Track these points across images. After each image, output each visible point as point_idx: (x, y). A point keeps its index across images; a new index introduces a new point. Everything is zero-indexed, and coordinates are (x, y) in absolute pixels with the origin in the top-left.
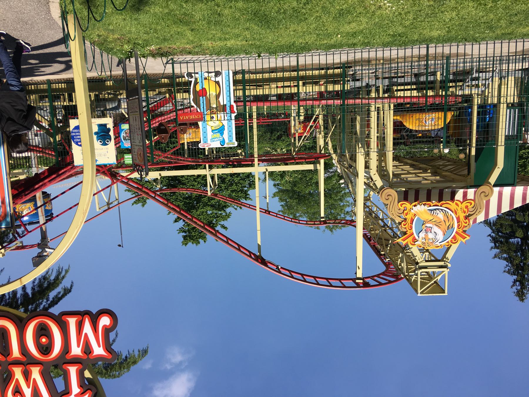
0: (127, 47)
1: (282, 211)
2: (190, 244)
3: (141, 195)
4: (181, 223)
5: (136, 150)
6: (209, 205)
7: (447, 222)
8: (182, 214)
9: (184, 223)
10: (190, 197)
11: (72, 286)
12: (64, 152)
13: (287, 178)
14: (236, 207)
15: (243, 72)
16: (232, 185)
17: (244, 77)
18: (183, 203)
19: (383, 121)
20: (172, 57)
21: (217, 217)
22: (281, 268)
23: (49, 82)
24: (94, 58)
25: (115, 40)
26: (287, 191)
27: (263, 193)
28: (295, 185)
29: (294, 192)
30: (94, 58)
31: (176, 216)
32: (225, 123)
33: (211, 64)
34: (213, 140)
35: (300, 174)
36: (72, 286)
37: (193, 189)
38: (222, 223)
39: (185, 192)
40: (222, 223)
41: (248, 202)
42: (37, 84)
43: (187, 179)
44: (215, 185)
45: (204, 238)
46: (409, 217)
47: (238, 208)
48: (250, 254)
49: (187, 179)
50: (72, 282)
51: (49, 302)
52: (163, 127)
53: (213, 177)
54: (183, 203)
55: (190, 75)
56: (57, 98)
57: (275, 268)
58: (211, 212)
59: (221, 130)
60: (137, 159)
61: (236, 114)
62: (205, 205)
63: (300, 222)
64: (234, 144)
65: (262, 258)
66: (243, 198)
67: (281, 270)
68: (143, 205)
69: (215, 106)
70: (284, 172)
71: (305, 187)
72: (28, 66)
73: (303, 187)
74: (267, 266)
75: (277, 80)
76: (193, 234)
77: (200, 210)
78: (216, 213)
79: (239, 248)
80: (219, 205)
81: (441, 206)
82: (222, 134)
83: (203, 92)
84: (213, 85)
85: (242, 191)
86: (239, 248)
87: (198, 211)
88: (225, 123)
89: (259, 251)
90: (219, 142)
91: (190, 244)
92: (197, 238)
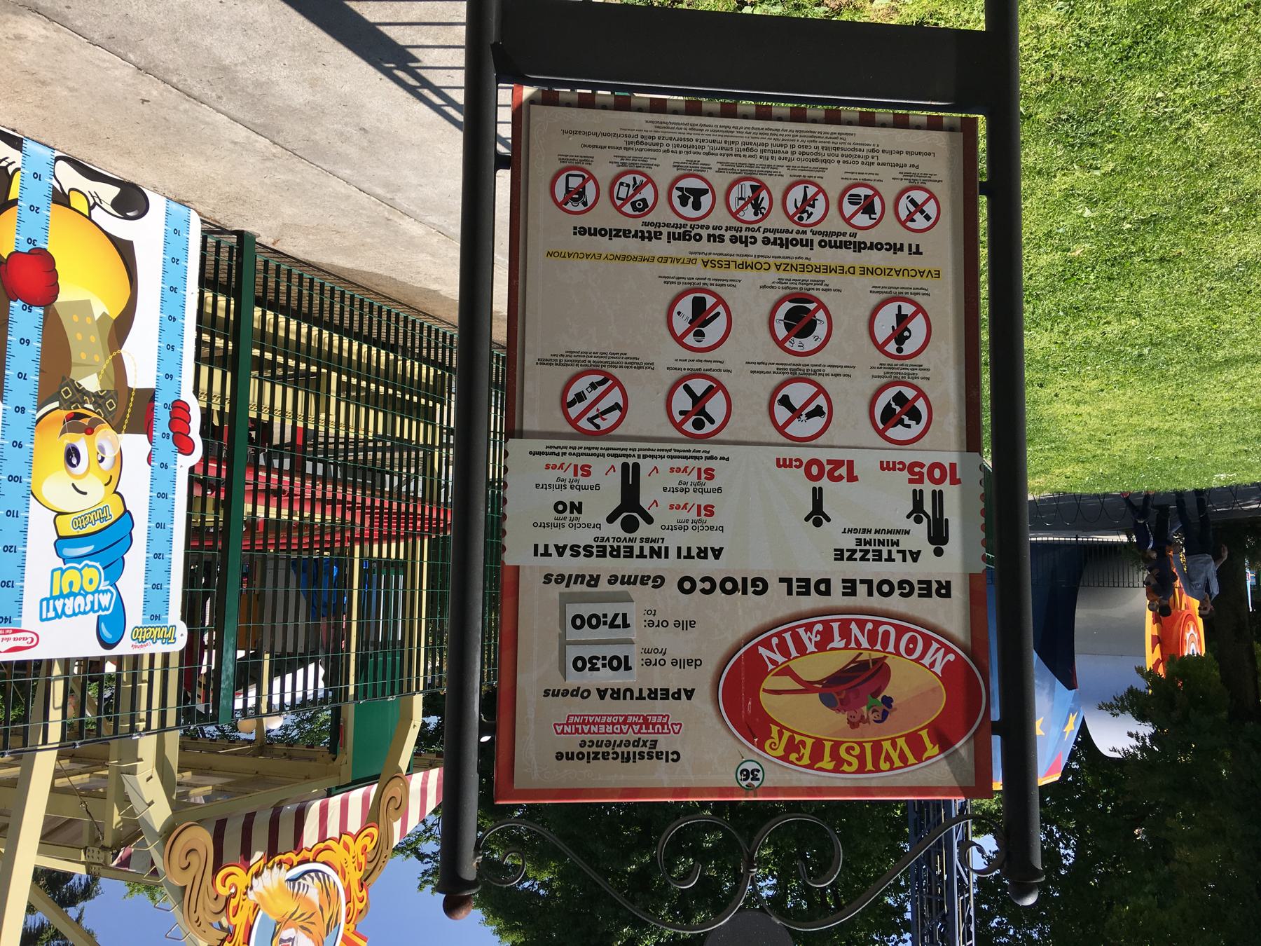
7: (326, 908)
46: (239, 921)
69: (91, 383)
81: (314, 861)
82: (114, 568)
90: (93, 618)
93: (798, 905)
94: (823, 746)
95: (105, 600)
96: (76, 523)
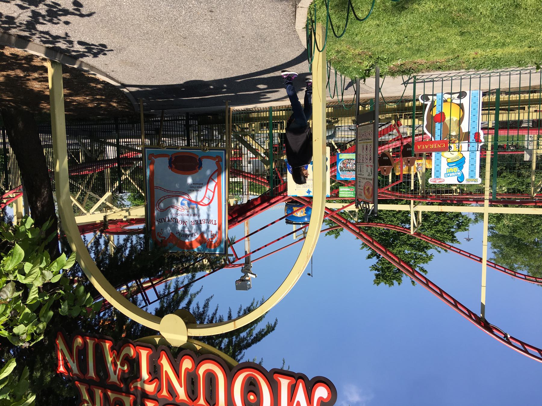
0: (366, 64)
1: (495, 260)
2: (382, 284)
3: (339, 226)
4: (374, 260)
5: (362, 184)
6: (407, 244)
8: (388, 255)
9: (377, 260)
10: (387, 234)
11: (275, 324)
12: (276, 181)
13: (505, 222)
14: (439, 249)
15: (498, 92)
16: (436, 224)
17: (498, 98)
18: (379, 239)
19: (483, 160)
20: (415, 74)
21: (416, 258)
22: (511, 337)
23: (271, 110)
24: (329, 78)
25: (354, 56)
26: (503, 236)
27: (479, 238)
28: (515, 231)
29: (512, 238)
30: (329, 78)
31: (370, 252)
32: (467, 155)
33: (456, 83)
34: (447, 175)
35: (524, 218)
36: (275, 324)
37: (391, 225)
38: (421, 265)
39: (382, 228)
40: (421, 265)
41: (455, 245)
42: (259, 111)
43: (385, 214)
44: (419, 223)
45: (399, 280)
47: (443, 251)
48: (470, 314)
49: (385, 214)
50: (276, 320)
51: (252, 338)
52: (386, 158)
53: (416, 213)
54: (379, 239)
55: (425, 97)
56: (275, 126)
57: (502, 336)
58: (409, 252)
59: (460, 163)
60: (363, 194)
61: (482, 144)
62: (405, 243)
63: (517, 275)
64: (476, 180)
65: (486, 321)
66: (450, 240)
67: (511, 340)
68: (336, 237)
70: (501, 214)
71: (529, 234)
72: (256, 92)
73: (526, 234)
74: (492, 332)
75: (531, 102)
76: (387, 274)
77: (396, 249)
78: (415, 254)
79: (456, 304)
80: (419, 246)
82: (461, 167)
83: (441, 117)
84: (456, 110)
85: (448, 232)
86: (456, 304)
87: (395, 250)
88: (467, 155)
89: (483, 312)
91: (382, 284)
92: (390, 279)
93: (248, 276)
94: (149, 373)
95: (459, 174)
96: (451, 160)
